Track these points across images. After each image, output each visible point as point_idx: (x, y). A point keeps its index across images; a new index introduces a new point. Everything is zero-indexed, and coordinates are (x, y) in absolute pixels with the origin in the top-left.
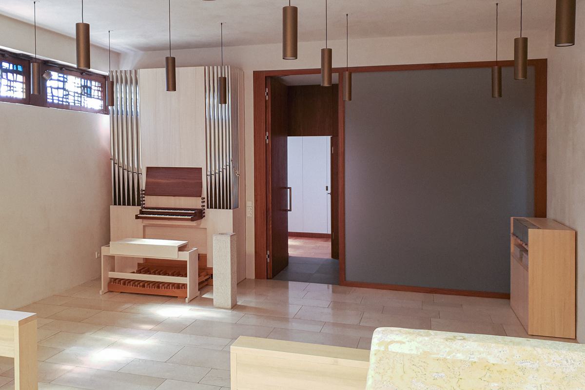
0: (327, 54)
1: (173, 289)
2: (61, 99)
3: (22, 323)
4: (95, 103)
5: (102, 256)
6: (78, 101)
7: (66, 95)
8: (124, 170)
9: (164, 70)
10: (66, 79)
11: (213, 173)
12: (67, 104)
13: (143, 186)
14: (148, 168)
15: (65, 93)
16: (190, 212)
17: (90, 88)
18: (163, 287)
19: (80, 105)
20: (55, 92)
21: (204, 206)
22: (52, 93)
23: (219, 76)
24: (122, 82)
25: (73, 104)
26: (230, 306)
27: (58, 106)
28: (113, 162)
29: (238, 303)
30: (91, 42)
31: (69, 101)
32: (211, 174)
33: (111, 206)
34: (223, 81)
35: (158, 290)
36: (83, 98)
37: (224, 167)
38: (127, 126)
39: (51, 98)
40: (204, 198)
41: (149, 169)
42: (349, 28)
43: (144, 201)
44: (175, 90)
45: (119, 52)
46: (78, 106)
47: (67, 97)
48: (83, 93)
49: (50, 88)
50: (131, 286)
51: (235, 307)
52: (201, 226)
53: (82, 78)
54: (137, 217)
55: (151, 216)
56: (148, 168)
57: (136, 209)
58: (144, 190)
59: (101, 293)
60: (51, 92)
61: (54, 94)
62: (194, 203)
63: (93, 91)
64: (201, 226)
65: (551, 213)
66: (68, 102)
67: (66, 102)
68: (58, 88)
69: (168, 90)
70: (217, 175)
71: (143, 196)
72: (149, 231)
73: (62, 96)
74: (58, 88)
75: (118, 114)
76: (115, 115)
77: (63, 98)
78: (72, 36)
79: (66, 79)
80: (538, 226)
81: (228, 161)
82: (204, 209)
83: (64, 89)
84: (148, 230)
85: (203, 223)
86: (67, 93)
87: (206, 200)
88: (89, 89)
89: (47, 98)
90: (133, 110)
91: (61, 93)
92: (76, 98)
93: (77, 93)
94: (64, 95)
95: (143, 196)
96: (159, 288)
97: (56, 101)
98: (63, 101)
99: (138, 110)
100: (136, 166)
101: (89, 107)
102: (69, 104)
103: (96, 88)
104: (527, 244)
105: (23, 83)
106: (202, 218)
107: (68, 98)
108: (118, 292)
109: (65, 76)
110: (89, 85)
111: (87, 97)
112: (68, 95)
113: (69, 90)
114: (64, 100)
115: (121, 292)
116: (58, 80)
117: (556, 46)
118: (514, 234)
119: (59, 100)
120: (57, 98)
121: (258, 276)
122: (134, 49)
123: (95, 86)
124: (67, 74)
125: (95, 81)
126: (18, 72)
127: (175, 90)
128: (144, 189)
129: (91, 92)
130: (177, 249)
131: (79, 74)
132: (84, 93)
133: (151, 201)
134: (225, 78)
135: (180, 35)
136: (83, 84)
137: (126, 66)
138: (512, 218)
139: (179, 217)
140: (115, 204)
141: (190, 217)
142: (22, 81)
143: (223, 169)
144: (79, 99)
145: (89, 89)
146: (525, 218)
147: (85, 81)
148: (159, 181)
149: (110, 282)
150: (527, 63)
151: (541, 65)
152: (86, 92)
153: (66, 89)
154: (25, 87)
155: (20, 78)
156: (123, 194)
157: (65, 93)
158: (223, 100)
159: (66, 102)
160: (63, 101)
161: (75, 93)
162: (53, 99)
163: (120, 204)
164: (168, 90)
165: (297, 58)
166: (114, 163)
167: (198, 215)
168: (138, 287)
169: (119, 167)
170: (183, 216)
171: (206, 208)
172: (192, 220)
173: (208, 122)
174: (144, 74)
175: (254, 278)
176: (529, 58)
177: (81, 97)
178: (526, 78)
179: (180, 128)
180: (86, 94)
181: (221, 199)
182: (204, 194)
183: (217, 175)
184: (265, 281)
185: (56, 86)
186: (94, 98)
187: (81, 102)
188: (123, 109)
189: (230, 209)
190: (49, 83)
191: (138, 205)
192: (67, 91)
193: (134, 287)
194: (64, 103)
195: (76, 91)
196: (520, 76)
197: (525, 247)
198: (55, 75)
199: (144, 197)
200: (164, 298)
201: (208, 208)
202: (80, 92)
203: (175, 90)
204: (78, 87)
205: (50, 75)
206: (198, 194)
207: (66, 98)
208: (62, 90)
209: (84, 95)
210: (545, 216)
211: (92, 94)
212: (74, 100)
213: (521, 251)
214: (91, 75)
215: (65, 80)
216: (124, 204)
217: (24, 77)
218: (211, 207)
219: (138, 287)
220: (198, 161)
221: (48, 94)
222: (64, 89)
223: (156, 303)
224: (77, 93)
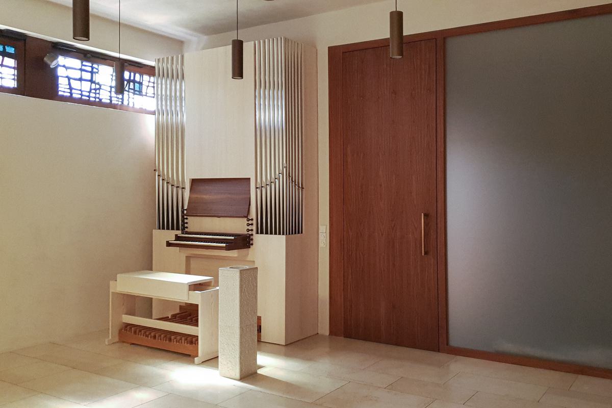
0: (397, 19)
1: (186, 344)
5: (110, 293)
7: (95, 89)
15: (93, 86)
17: (140, 84)
18: (175, 340)
19: (120, 103)
21: (252, 230)
22: (69, 84)
26: (238, 376)
30: (91, 12)
31: (100, 97)
35: (154, 340)
39: (69, 91)
40: (252, 220)
45: (182, 40)
47: (98, 91)
49: (67, 79)
50: (142, 336)
52: (250, 258)
54: (169, 244)
57: (171, 235)
59: (107, 343)
62: (237, 226)
68: (81, 79)
73: (89, 90)
77: (90, 92)
78: (68, 5)
82: (252, 235)
83: (92, 81)
84: (194, 264)
86: (98, 87)
87: (254, 222)
88: (137, 85)
91: (86, 86)
94: (91, 89)
96: (136, 334)
97: (76, 95)
98: (89, 96)
105: (14, 68)
107: (99, 94)
108: (128, 343)
109: (95, 66)
111: (134, 94)
112: (99, 89)
113: (100, 83)
114: (92, 95)
119: (82, 95)
120: (80, 92)
121: (333, 332)
122: (191, 32)
124: (98, 63)
126: (10, 55)
130: (187, 288)
131: (82, 55)
132: (129, 88)
133: (196, 224)
142: (13, 65)
148: (204, 196)
149: (126, 327)
154: (16, 74)
155: (11, 62)
156: (172, 219)
160: (89, 96)
167: (243, 242)
168: (149, 338)
171: (254, 232)
172: (228, 248)
174: (193, 58)
179: (227, 126)
180: (132, 91)
182: (253, 214)
185: (79, 77)
186: (146, 95)
187: (122, 99)
189: (283, 234)
190: (61, 72)
192: (98, 84)
193: (144, 337)
200: (170, 354)
201: (257, 233)
206: (246, 216)
207: (95, 93)
208: (90, 83)
209: (128, 91)
212: (111, 97)
214: (141, 67)
215: (95, 70)
217: (16, 61)
218: (262, 233)
219: (149, 338)
222: (92, 81)
223: (210, 366)
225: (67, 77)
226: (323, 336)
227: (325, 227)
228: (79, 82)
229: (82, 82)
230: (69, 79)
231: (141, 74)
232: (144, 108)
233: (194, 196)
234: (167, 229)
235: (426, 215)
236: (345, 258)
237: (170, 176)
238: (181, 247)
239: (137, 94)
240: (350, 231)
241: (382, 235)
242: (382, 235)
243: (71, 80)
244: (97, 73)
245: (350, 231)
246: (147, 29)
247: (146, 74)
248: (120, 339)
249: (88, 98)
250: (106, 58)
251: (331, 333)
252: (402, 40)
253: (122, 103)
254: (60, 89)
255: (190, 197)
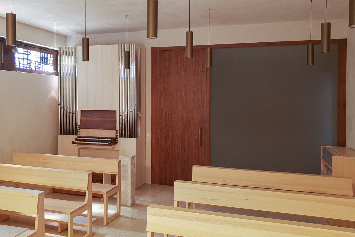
0: (190, 36)
2: (25, 66)
3: (40, 195)
4: (49, 68)
6: (38, 67)
7: (29, 63)
8: (67, 112)
9: (81, 47)
10: (30, 53)
11: (123, 114)
12: (30, 69)
13: (79, 122)
14: (82, 111)
15: (29, 62)
16: (108, 140)
17: (47, 59)
19: (39, 70)
20: (21, 61)
21: (117, 136)
22: (19, 62)
23: (126, 51)
24: (66, 55)
25: (34, 69)
27: (24, 70)
28: (60, 106)
29: (136, 203)
31: (31, 67)
32: (122, 115)
33: (58, 135)
34: (127, 54)
36: (41, 65)
37: (131, 110)
38: (69, 82)
39: (19, 65)
40: (118, 131)
41: (82, 111)
42: (211, 18)
43: (79, 132)
44: (89, 60)
46: (38, 70)
47: (30, 64)
48: (41, 62)
49: (18, 59)
51: (134, 205)
52: (116, 149)
53: (41, 52)
54: (73, 143)
55: (83, 142)
56: (82, 111)
57: (73, 138)
58: (79, 125)
60: (18, 61)
61: (20, 63)
62: (110, 134)
63: (48, 60)
64: (116, 149)
65: (348, 143)
66: (30, 68)
67: (29, 68)
68: (24, 59)
69: (83, 60)
70: (126, 115)
71: (79, 129)
72: (82, 152)
73: (27, 64)
74: (24, 59)
75: (66, 75)
76: (62, 76)
77: (27, 65)
79: (30, 53)
80: (339, 153)
81: (133, 106)
82: (118, 138)
83: (28, 59)
84: (82, 152)
85: (117, 147)
86: (30, 62)
87: (118, 132)
88: (46, 59)
89: (15, 65)
90: (73, 72)
91: (26, 62)
92: (37, 65)
93: (37, 62)
94: (28, 63)
95: (79, 129)
97: (22, 67)
98: (27, 67)
99: (76, 73)
100: (74, 110)
101: (46, 71)
102: (31, 69)
103: (51, 59)
104: (331, 166)
106: (116, 144)
107: (31, 65)
108: (59, 193)
109: (29, 51)
110: (46, 56)
111: (45, 64)
112: (31, 63)
113: (31, 60)
114: (28, 66)
115: (61, 193)
116: (24, 54)
117: (349, 27)
118: (323, 158)
119: (24, 67)
120: (23, 65)
121: (153, 182)
122: (74, 33)
123: (50, 57)
125: (51, 54)
127: (88, 60)
128: (79, 124)
129: (47, 61)
132: (43, 62)
133: (83, 132)
134: (129, 52)
135: (93, 24)
136: (42, 56)
137: (71, 44)
138: (322, 147)
139: (100, 143)
140: (61, 134)
141: (107, 143)
143: (130, 111)
144: (39, 66)
145: (46, 59)
146: (330, 147)
147: (187, 55)
150: (330, 42)
151: (342, 43)
152: (43, 61)
153: (30, 59)
156: (67, 127)
157: (29, 62)
158: (127, 66)
159: (29, 68)
160: (27, 67)
161: (36, 62)
162: (20, 66)
163: (64, 134)
164: (83, 60)
165: (157, 38)
166: (61, 107)
167: (113, 142)
169: (64, 110)
170: (103, 142)
171: (118, 137)
172: (109, 145)
173: (120, 80)
175: (150, 183)
176: (331, 38)
177: (40, 64)
178: (329, 52)
180: (43, 63)
181: (129, 130)
183: (126, 115)
184: (157, 186)
185: (22, 58)
186: (49, 65)
187: (40, 67)
188: (70, 72)
189: (134, 138)
190: (17, 55)
191: (75, 135)
192: (30, 60)
194: (28, 69)
195: (37, 61)
196: (325, 51)
197: (330, 168)
198: (20, 50)
199: (79, 130)
201: (120, 137)
202: (39, 61)
203: (89, 60)
204: (38, 58)
205: (16, 50)
206: (114, 128)
207: (29, 65)
208: (27, 60)
209: (42, 63)
210: (345, 146)
211: (48, 62)
212: (35, 67)
213: (327, 170)
215: (29, 53)
216: (67, 134)
218: (122, 137)
220: (115, 108)
221: (16, 63)
222: (28, 59)
224: (37, 62)
225: (18, 58)
226: (148, 184)
227: (149, 133)
228: (23, 60)
229: (24, 60)
230: (19, 59)
231: (47, 54)
232: (48, 71)
233: (84, 118)
234: (66, 134)
235: (201, 129)
236: (160, 148)
237: (74, 110)
238: (78, 144)
239: (46, 64)
240: (162, 135)
241: (179, 137)
242: (179, 137)
243: (20, 59)
244: (30, 54)
245: (162, 135)
246: (48, 30)
247: (49, 53)
248: (53, 191)
249: (26, 68)
250: (34, 46)
251: (152, 183)
252: (193, 48)
253: (40, 70)
254: (16, 64)
255: (81, 119)
